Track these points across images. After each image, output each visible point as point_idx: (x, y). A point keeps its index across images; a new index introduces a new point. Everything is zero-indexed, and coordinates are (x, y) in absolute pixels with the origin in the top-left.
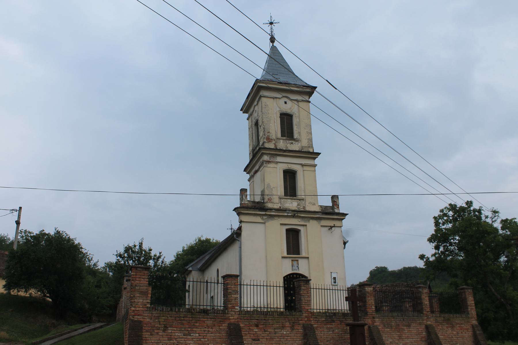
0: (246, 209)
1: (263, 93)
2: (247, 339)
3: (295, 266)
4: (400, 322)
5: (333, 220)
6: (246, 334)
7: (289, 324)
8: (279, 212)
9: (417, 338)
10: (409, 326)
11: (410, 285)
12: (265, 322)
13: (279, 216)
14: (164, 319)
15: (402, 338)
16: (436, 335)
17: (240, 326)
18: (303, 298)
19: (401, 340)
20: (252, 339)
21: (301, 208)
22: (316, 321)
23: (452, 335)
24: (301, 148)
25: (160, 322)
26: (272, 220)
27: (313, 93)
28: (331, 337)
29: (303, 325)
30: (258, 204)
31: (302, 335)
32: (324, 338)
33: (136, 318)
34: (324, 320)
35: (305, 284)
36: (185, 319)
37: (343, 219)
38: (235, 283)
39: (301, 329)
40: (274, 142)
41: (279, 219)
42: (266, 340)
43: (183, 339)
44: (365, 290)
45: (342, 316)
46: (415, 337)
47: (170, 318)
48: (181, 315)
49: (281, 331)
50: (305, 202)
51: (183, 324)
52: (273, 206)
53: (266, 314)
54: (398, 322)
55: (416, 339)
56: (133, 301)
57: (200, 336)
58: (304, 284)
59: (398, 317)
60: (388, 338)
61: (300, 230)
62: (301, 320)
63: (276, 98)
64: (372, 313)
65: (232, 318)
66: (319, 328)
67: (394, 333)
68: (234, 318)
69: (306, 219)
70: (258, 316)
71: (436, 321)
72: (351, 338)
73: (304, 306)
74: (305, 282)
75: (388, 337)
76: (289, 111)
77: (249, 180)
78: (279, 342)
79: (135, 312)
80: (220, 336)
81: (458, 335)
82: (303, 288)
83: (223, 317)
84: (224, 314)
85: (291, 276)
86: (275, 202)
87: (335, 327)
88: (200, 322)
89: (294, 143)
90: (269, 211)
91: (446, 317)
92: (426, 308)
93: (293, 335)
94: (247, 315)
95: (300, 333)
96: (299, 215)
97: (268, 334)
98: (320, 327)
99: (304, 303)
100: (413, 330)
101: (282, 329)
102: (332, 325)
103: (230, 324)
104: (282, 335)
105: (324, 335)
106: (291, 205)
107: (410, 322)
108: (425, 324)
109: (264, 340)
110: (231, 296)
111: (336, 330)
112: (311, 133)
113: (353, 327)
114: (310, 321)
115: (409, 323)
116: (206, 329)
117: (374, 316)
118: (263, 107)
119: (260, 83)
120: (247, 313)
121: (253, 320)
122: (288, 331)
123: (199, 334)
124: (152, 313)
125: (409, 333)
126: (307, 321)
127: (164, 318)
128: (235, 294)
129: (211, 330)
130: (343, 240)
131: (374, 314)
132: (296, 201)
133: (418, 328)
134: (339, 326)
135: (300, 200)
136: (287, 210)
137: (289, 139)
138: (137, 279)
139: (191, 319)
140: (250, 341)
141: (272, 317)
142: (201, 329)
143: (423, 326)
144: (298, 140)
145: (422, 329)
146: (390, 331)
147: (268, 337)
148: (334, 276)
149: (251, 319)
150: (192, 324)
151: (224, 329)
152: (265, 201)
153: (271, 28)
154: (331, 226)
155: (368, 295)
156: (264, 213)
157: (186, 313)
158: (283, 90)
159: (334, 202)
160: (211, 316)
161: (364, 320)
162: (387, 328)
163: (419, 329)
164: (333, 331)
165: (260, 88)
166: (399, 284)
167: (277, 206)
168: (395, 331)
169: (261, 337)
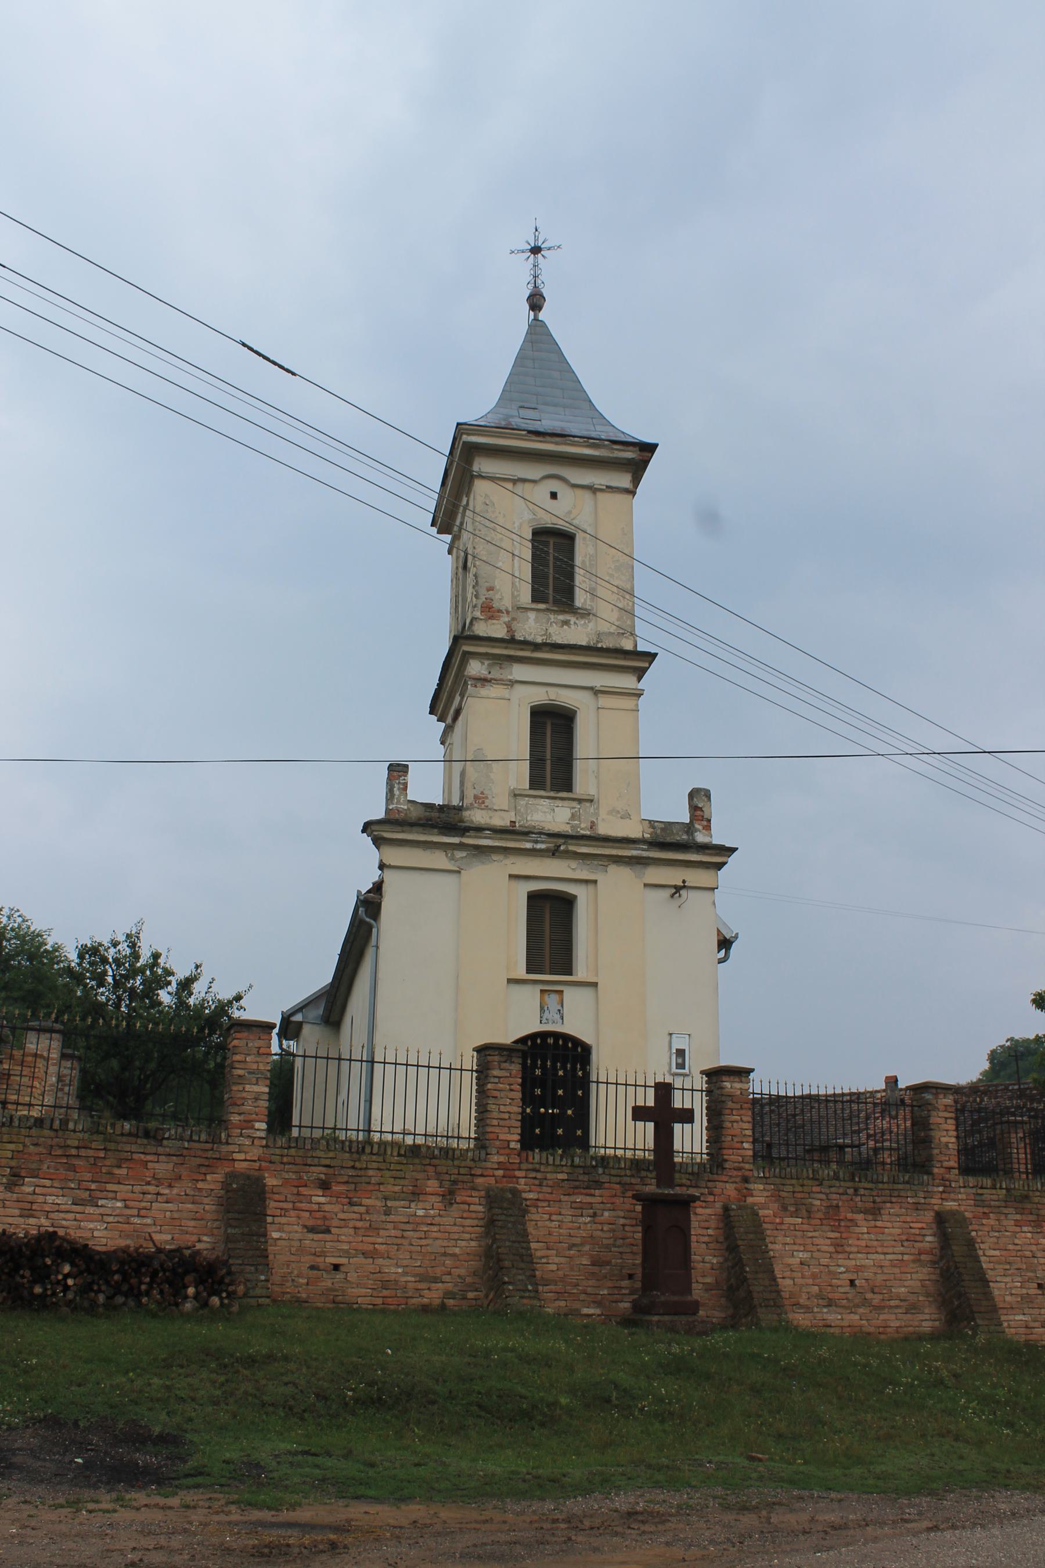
0: (400, 828)
1: (483, 465)
2: (288, 1224)
3: (550, 1008)
4: (844, 1197)
5: (688, 867)
6: (286, 1210)
7: (437, 1185)
8: (507, 839)
9: (902, 1254)
10: (875, 1212)
11: (1028, 1092)
12: (352, 1176)
14: (13, 1151)
15: (848, 1249)
16: (971, 1243)
17: (265, 1185)
18: (494, 1107)
19: (840, 1256)
20: (305, 1226)
21: (583, 826)
22: (537, 1182)
23: (1034, 1248)
24: (595, 639)
26: (483, 863)
27: (645, 463)
28: (584, 1235)
29: (488, 1190)
30: (443, 812)
31: (481, 1223)
32: (560, 1235)
34: (563, 1180)
35: (505, 1062)
36: (83, 1152)
38: (260, 1048)
39: (480, 1204)
40: (506, 618)
42: (352, 1231)
43: (73, 1214)
44: (722, 1088)
45: (630, 1169)
46: (896, 1250)
48: (69, 1142)
50: (598, 808)
51: (73, 1169)
52: (491, 817)
53: (360, 1149)
54: (834, 1196)
55: (900, 1257)
58: (500, 1062)
59: (837, 1183)
60: (796, 1247)
61: (575, 897)
62: (482, 1175)
63: (524, 481)
64: (742, 1165)
65: (242, 1156)
66: (545, 1204)
67: (814, 1234)
68: (248, 1158)
69: (596, 862)
71: (979, 1202)
72: (645, 1239)
73: (497, 1130)
77: (443, 743)
78: (399, 1241)
80: (197, 1212)
82: (496, 1072)
83: (210, 1154)
84: (213, 1143)
85: (539, 1041)
87: (602, 1203)
88: (131, 1166)
89: (572, 622)
90: (472, 833)
91: (1014, 1189)
92: (944, 1158)
93: (451, 1220)
94: (293, 1151)
95: (474, 1215)
96: (571, 848)
97: (361, 1214)
98: (549, 1201)
99: (495, 1122)
100: (889, 1224)
101: (413, 1201)
102: (593, 1195)
103: (232, 1176)
104: (411, 1219)
106: (549, 817)
107: (878, 1199)
108: (936, 1208)
109: (345, 1230)
110: (241, 1089)
111: (606, 1214)
113: (650, 1203)
114: (514, 1179)
115: (874, 1202)
116: (151, 1189)
117: (747, 1173)
119: (469, 434)
120: (293, 1145)
121: (315, 1165)
122: (433, 1209)
123: (125, 1201)
125: (873, 1237)
127: (12, 1146)
128: (257, 1084)
129: (166, 1191)
130: (719, 932)
131: (747, 1166)
132: (566, 803)
133: (908, 1219)
134: (618, 1201)
135: (580, 801)
136: (533, 833)
137: (555, 608)
139: (102, 1154)
140: (296, 1232)
141: (381, 1159)
143: (929, 1216)
145: (920, 1225)
146: (805, 1227)
147: (359, 1224)
148: (677, 1044)
149: (306, 1165)
150: (104, 1171)
151: (212, 1190)
152: (467, 802)
153: (535, 266)
155: (730, 1104)
156: (455, 840)
157: (86, 1136)
158: (536, 454)
159: (695, 810)
160: (168, 1147)
161: (710, 1184)
162: (795, 1214)
163: (912, 1225)
164: (595, 1215)
167: (503, 819)
168: (822, 1225)
169: (335, 1222)
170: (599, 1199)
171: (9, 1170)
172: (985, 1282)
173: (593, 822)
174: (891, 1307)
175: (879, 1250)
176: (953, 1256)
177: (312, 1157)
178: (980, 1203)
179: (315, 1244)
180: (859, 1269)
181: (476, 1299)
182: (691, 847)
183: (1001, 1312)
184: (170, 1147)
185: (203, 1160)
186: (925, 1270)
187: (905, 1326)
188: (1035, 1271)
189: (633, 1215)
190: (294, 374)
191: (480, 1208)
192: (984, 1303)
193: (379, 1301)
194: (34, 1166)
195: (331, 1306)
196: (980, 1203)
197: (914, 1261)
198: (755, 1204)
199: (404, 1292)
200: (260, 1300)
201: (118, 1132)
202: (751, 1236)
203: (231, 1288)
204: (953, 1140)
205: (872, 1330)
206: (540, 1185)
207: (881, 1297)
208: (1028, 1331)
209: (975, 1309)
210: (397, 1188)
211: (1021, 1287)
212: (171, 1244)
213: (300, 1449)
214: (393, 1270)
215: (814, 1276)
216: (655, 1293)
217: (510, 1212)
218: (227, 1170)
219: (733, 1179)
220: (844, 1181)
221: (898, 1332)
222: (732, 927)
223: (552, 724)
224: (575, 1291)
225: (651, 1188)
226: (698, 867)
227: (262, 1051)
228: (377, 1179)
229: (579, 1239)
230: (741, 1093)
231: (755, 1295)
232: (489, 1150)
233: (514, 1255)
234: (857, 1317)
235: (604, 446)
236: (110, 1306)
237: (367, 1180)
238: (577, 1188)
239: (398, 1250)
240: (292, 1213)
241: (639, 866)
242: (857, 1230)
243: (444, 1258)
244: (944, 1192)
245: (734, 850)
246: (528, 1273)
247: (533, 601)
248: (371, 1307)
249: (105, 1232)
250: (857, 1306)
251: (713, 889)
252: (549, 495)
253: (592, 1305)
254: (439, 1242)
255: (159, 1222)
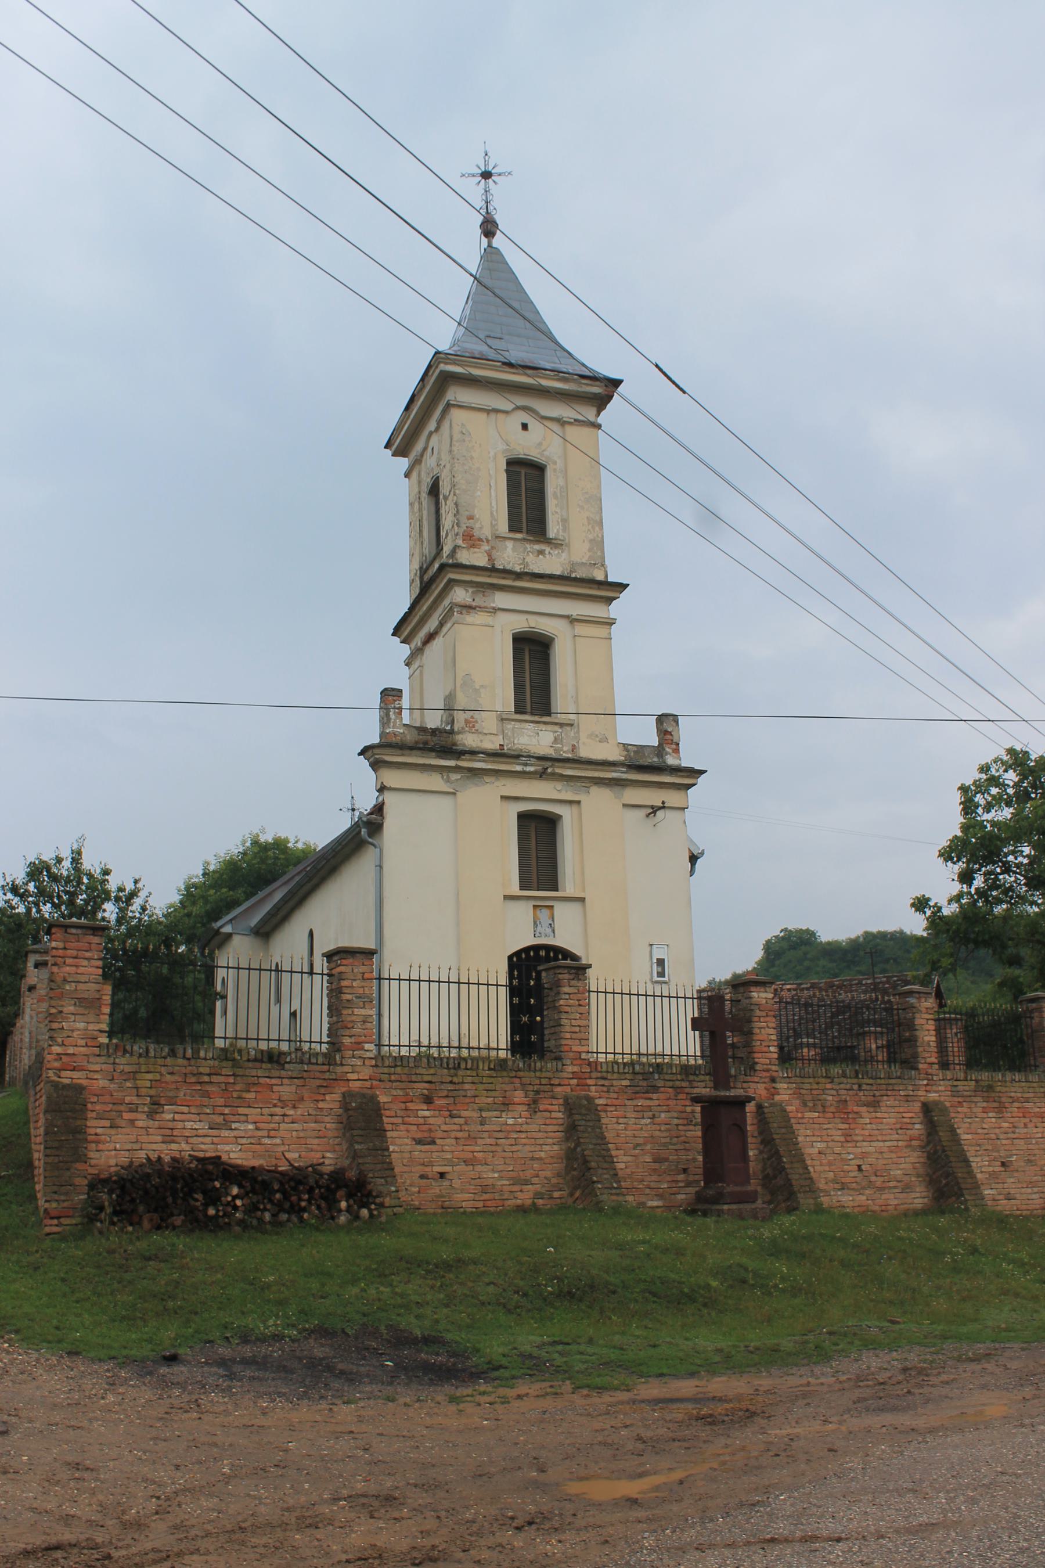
0: (400, 752)
4: (851, 1092)
7: (523, 1095)
10: (874, 1104)
13: (497, 773)
14: (151, 1081)
15: (855, 1138)
17: (379, 1102)
18: (566, 1021)
19: (849, 1145)
20: (414, 1139)
21: (565, 749)
22: (605, 1089)
24: (569, 568)
25: (137, 1088)
26: (477, 785)
27: (610, 398)
29: (566, 1099)
31: (561, 1128)
33: (67, 1077)
34: (627, 1086)
35: (573, 979)
36: (214, 1079)
37: (689, 786)
38: (364, 973)
39: (560, 1112)
41: (497, 783)
42: (453, 1141)
43: (210, 1138)
44: (751, 998)
47: (168, 1076)
48: (201, 1070)
49: (501, 1117)
50: (578, 732)
51: (207, 1095)
52: (481, 741)
55: (895, 1143)
56: (55, 1026)
57: (257, 1129)
59: (844, 1080)
60: (815, 1139)
61: (560, 817)
62: (559, 1085)
63: (497, 411)
64: (770, 1067)
65: (354, 1076)
66: (612, 1109)
69: (579, 784)
70: (432, 1071)
71: (955, 1092)
74: (573, 971)
75: (813, 1136)
76: (534, 454)
78: (493, 1148)
79: (65, 1059)
81: (1014, 1132)
82: (566, 989)
83: (327, 1075)
84: (329, 1064)
85: (532, 954)
86: (485, 731)
88: (260, 1090)
89: (547, 552)
90: (467, 756)
91: (982, 1080)
94: (399, 1070)
95: (555, 1121)
96: (557, 770)
97: (461, 1125)
99: (568, 1036)
100: (886, 1115)
102: (651, 1099)
105: (626, 1129)
106: (534, 741)
107: (877, 1093)
108: (922, 1099)
109: (448, 1140)
111: (663, 1115)
112: (600, 524)
114: (586, 1087)
117: (775, 1074)
118: (455, 438)
119: (446, 363)
120: (399, 1063)
122: (520, 1117)
124: (114, 1063)
125: (874, 1126)
126: (578, 1088)
127: (150, 1076)
128: (364, 1007)
129: (291, 1112)
131: (774, 1068)
132: (549, 727)
134: (672, 1103)
135: (561, 725)
136: (523, 756)
137: (531, 538)
138: (69, 961)
140: (407, 1144)
142: (261, 1108)
143: (917, 1107)
144: (560, 542)
145: (910, 1115)
146: (821, 1120)
147: (460, 1135)
148: (658, 954)
150: (235, 1096)
151: (331, 1109)
153: (486, 191)
154: (652, 807)
155: (758, 1013)
156: (452, 763)
157: (217, 1063)
159: (665, 734)
161: (745, 1085)
162: (813, 1109)
163: (904, 1115)
164: (654, 1117)
165: (447, 380)
166: (850, 980)
167: (493, 743)
169: (440, 1134)
170: (656, 1102)
171: (149, 1098)
172: (967, 1162)
173: (573, 746)
174: (890, 1188)
175: (880, 1138)
176: (940, 1141)
177: (416, 1074)
178: (954, 1093)
179: (423, 1155)
180: (864, 1155)
181: (560, 1198)
182: (665, 770)
183: (982, 1187)
184: (292, 1071)
185: (321, 1081)
186: (915, 1154)
187: (902, 1204)
188: (998, 1151)
189: (684, 1115)
190: (684, 392)
191: (560, 1115)
192: (969, 1180)
193: (480, 1204)
194: (171, 1094)
195: (440, 1211)
196: (954, 1093)
197: (906, 1147)
198: (782, 1101)
199: (501, 1195)
200: (395, 1210)
201: (245, 1058)
202: (783, 1130)
203: (378, 1200)
204: (934, 1039)
205: (877, 1208)
206: (608, 1092)
207: (882, 1179)
208: (995, 1203)
209: (963, 1186)
210: (490, 1100)
211: (989, 1166)
212: (298, 1161)
213: (550, 1339)
214: (491, 1175)
215: (830, 1164)
216: (720, 1184)
217: (588, 1117)
218: (344, 1090)
219: (763, 1080)
220: (851, 1078)
221: (896, 1209)
222: (700, 844)
223: (530, 650)
224: (641, 1186)
225: (704, 1089)
226: (670, 788)
227: (366, 976)
228: (472, 1092)
229: (642, 1139)
230: (766, 1002)
231: (794, 1182)
232: (564, 1062)
233: (597, 1156)
234: (864, 1198)
235: (574, 380)
236: (276, 1223)
237: (463, 1093)
238: (637, 1093)
239: (493, 1157)
240: (403, 1127)
241: (620, 787)
242: (862, 1121)
243: (532, 1162)
244: (927, 1085)
245: (703, 772)
246: (612, 1172)
247: (510, 530)
248: (474, 1210)
249: (240, 1153)
250: (864, 1188)
251: (684, 808)
252: (521, 427)
253: (655, 1198)
254: (527, 1148)
255: (286, 1142)
